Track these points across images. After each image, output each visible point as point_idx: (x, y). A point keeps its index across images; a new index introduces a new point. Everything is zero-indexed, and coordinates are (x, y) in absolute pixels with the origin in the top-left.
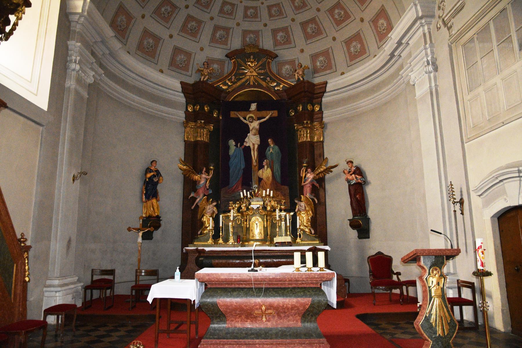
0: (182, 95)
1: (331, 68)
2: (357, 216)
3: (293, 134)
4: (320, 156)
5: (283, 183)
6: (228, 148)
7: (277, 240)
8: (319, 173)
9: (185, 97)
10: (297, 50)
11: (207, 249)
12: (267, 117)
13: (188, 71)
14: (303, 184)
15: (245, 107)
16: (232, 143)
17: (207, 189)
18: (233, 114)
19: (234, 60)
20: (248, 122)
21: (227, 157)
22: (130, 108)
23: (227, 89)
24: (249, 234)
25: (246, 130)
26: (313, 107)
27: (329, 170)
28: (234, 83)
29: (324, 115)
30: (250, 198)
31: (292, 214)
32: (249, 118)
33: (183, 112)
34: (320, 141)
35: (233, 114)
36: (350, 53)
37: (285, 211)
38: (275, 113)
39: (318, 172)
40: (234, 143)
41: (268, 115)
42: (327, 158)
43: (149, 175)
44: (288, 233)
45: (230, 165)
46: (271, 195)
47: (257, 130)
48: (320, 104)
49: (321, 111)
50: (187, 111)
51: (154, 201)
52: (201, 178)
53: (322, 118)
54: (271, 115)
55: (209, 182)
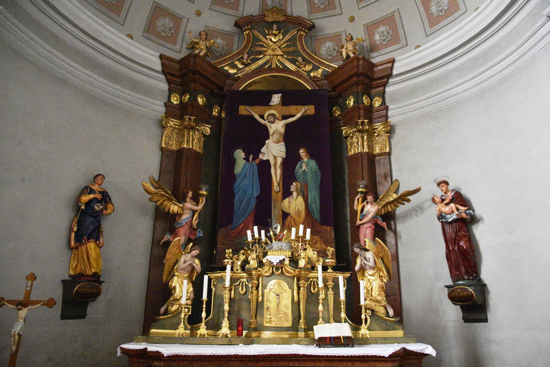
0: (163, 77)
1: (398, 41)
2: (464, 279)
3: (338, 143)
4: (386, 177)
5: (324, 221)
6: (232, 162)
7: (322, 330)
8: (388, 203)
9: (169, 82)
10: (345, 17)
11: (167, 350)
12: (298, 116)
13: (175, 43)
14: (358, 222)
15: (262, 98)
16: (240, 154)
17: (195, 230)
18: (243, 110)
19: (247, 32)
20: (267, 123)
21: (231, 177)
22: (64, 82)
23: (236, 74)
24: (262, 316)
25: (263, 134)
26: (371, 100)
27: (404, 198)
28: (246, 65)
29: (390, 113)
30: (266, 243)
31: (348, 275)
32: (268, 116)
33: (162, 104)
34: (385, 154)
35: (243, 110)
36: (429, 15)
37: (335, 269)
38: (310, 110)
39: (383, 203)
40: (243, 155)
41: (299, 112)
42: (397, 180)
43: (86, 198)
44: (343, 315)
45: (236, 191)
46: (308, 237)
47: (281, 134)
48: (383, 95)
49: (384, 107)
50: (168, 105)
51: (92, 245)
52: (183, 210)
53: (387, 117)
54: (305, 112)
55: (199, 216)
